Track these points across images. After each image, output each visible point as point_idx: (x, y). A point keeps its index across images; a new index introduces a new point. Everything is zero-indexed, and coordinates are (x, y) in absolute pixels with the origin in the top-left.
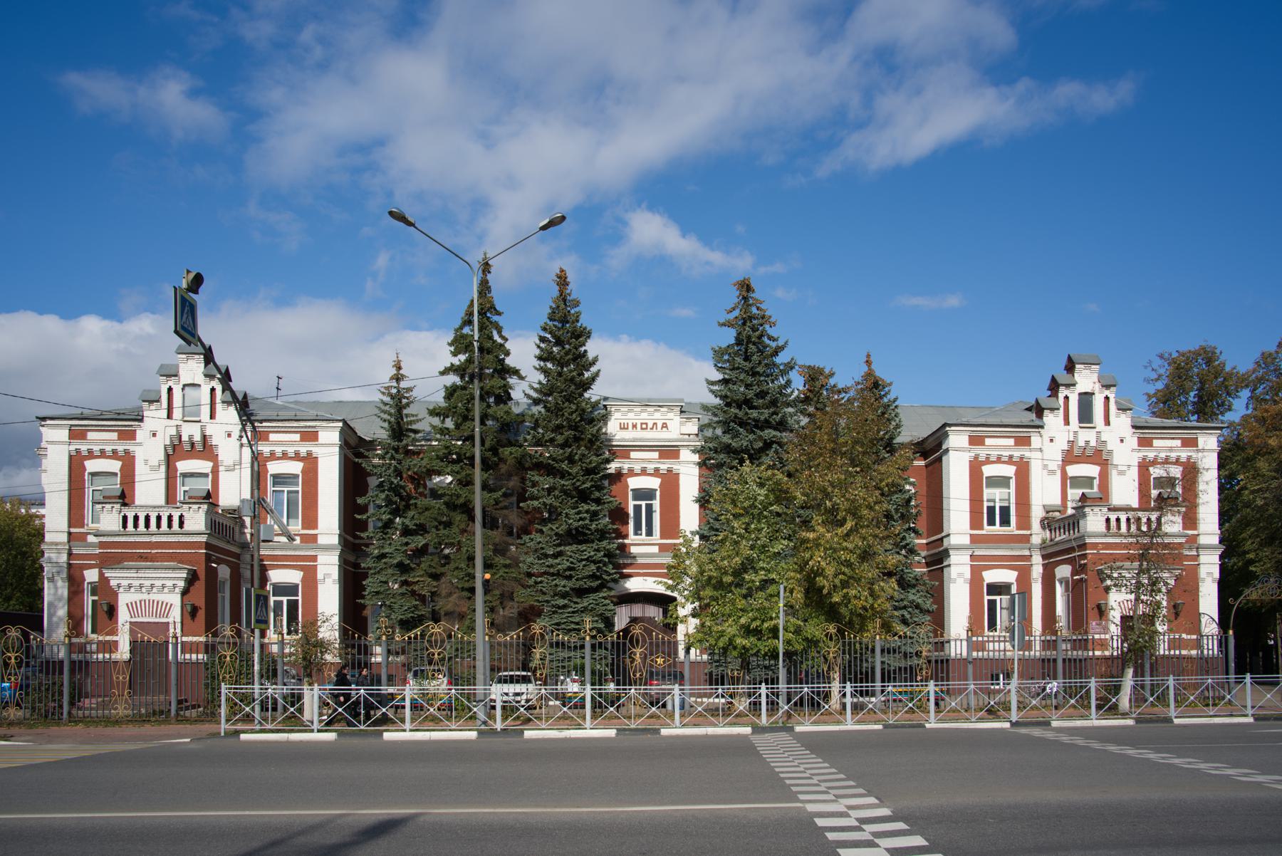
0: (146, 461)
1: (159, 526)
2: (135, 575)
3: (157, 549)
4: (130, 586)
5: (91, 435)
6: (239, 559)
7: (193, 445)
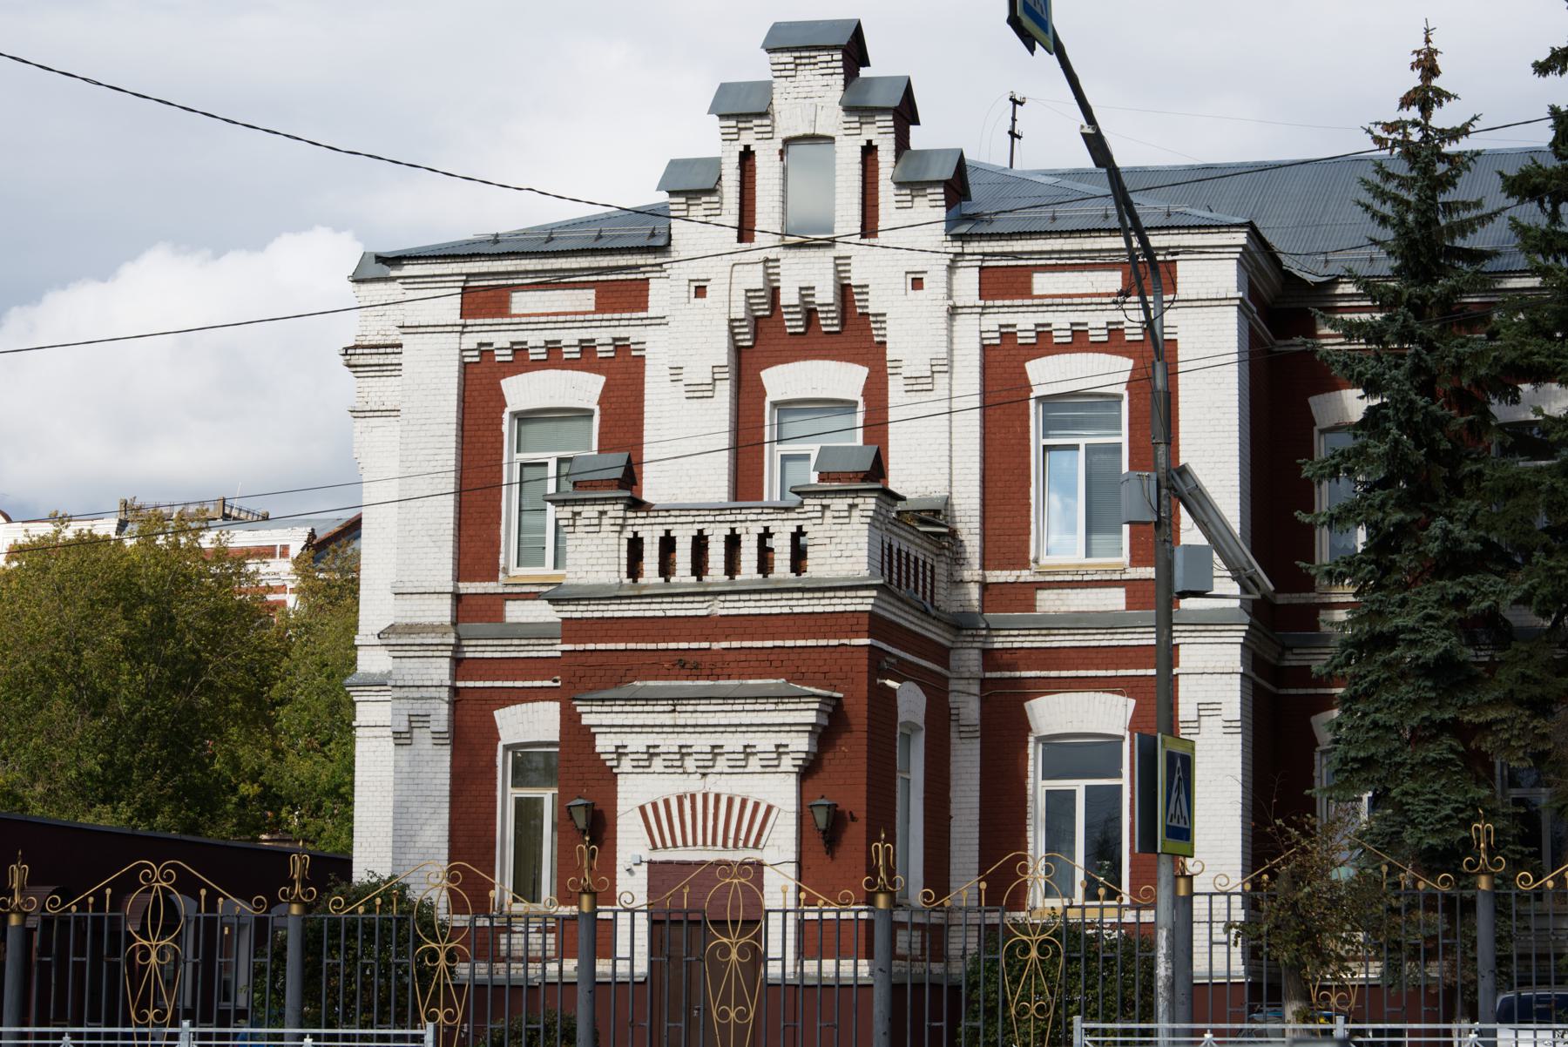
0: (676, 371)
1: (732, 567)
2: (667, 719)
3: (727, 638)
4: (651, 753)
5: (522, 302)
6: (946, 666)
7: (810, 314)
